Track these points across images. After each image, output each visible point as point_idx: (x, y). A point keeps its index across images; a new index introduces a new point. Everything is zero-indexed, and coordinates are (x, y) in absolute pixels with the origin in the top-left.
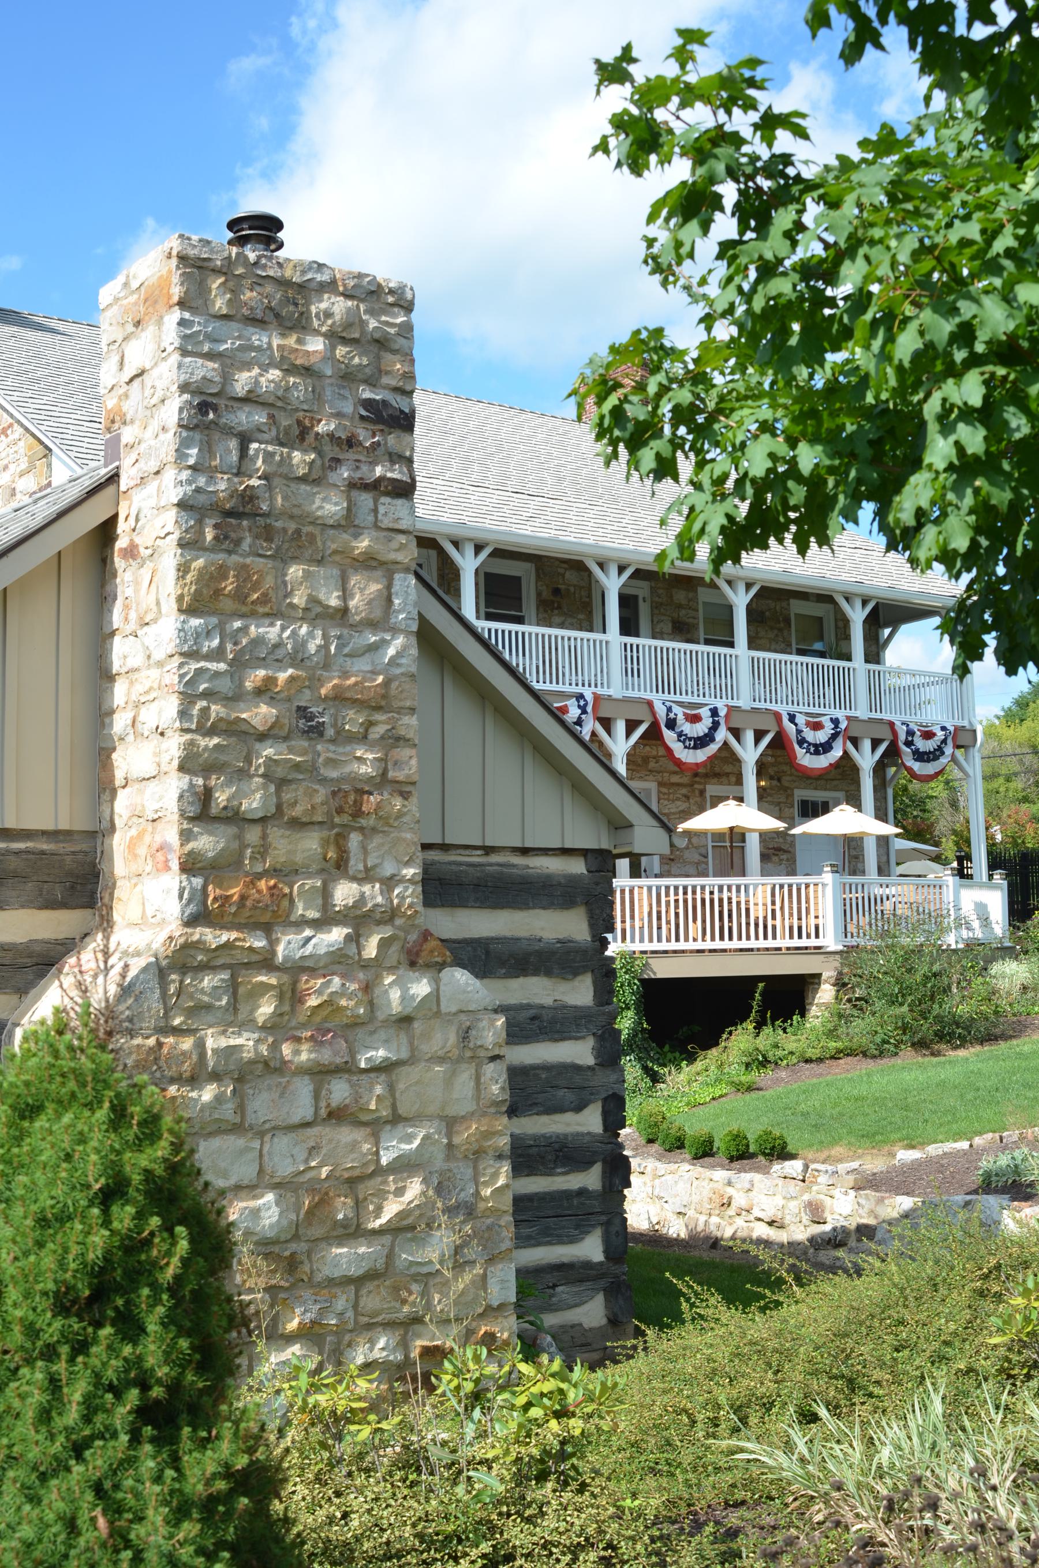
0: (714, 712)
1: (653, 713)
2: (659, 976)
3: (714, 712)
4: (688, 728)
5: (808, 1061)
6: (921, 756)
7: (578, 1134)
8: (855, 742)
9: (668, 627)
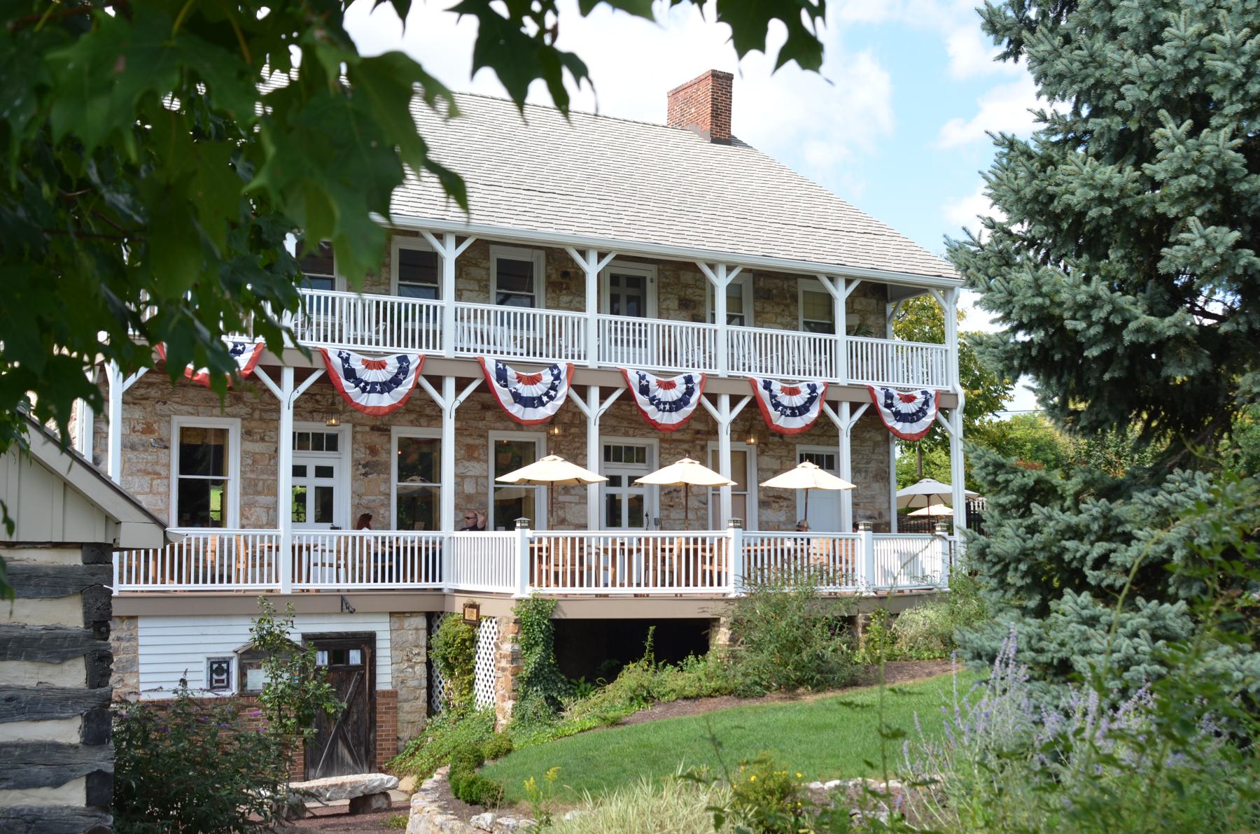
0: (689, 380)
1: (627, 381)
2: (569, 617)
3: (689, 380)
4: (661, 394)
5: (686, 698)
6: (900, 416)
7: (56, 807)
8: (835, 406)
9: (674, 304)
